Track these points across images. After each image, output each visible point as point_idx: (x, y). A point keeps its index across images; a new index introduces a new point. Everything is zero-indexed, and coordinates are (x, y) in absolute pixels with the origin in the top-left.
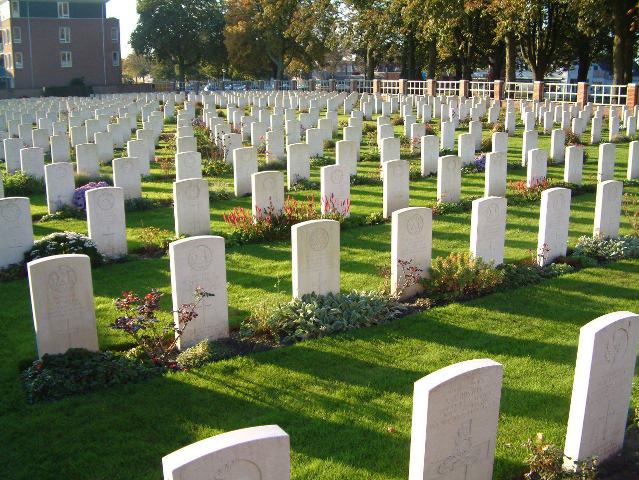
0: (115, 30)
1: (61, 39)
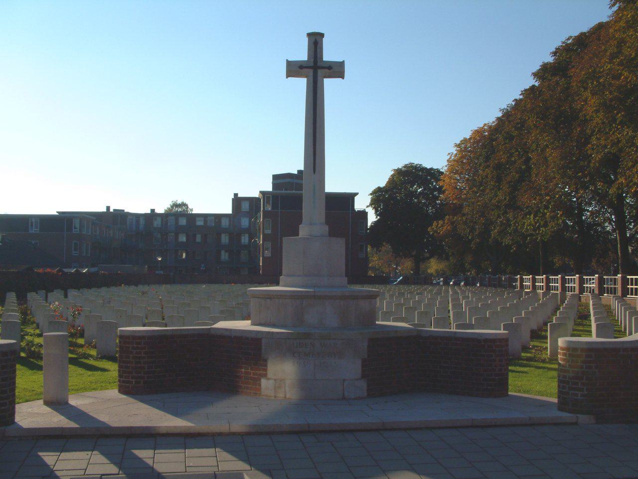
0: (363, 222)
1: (75, 252)
